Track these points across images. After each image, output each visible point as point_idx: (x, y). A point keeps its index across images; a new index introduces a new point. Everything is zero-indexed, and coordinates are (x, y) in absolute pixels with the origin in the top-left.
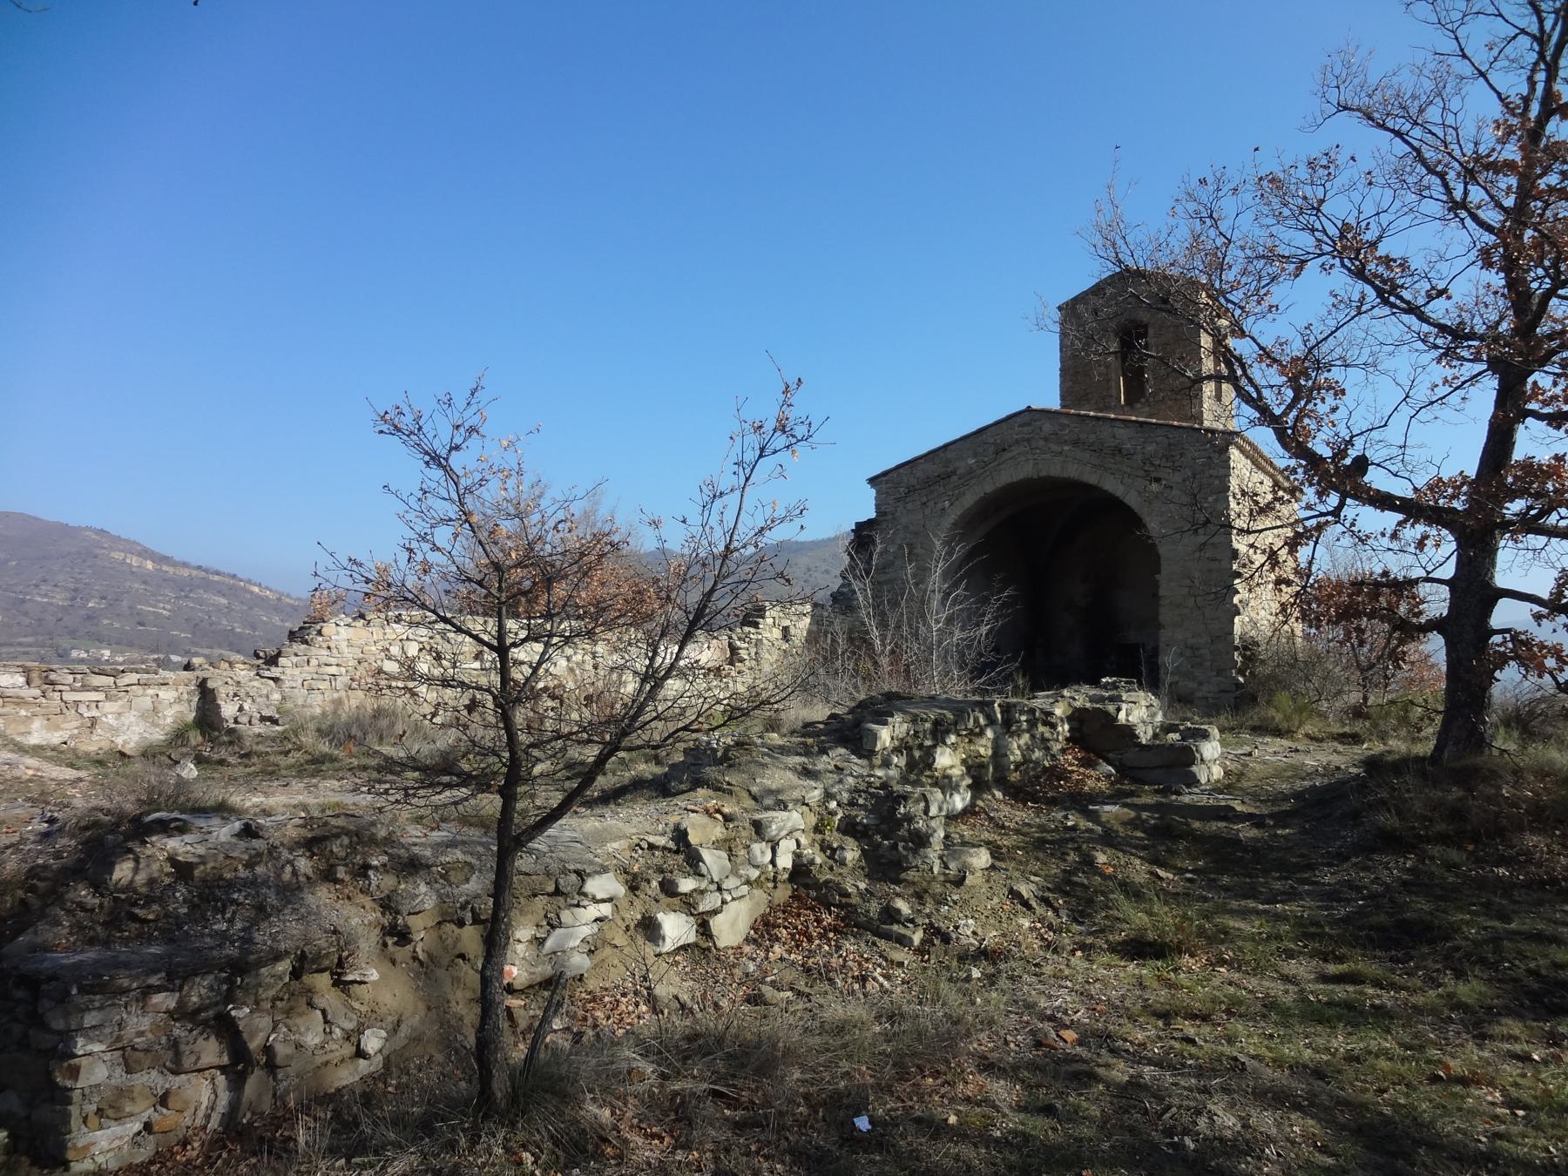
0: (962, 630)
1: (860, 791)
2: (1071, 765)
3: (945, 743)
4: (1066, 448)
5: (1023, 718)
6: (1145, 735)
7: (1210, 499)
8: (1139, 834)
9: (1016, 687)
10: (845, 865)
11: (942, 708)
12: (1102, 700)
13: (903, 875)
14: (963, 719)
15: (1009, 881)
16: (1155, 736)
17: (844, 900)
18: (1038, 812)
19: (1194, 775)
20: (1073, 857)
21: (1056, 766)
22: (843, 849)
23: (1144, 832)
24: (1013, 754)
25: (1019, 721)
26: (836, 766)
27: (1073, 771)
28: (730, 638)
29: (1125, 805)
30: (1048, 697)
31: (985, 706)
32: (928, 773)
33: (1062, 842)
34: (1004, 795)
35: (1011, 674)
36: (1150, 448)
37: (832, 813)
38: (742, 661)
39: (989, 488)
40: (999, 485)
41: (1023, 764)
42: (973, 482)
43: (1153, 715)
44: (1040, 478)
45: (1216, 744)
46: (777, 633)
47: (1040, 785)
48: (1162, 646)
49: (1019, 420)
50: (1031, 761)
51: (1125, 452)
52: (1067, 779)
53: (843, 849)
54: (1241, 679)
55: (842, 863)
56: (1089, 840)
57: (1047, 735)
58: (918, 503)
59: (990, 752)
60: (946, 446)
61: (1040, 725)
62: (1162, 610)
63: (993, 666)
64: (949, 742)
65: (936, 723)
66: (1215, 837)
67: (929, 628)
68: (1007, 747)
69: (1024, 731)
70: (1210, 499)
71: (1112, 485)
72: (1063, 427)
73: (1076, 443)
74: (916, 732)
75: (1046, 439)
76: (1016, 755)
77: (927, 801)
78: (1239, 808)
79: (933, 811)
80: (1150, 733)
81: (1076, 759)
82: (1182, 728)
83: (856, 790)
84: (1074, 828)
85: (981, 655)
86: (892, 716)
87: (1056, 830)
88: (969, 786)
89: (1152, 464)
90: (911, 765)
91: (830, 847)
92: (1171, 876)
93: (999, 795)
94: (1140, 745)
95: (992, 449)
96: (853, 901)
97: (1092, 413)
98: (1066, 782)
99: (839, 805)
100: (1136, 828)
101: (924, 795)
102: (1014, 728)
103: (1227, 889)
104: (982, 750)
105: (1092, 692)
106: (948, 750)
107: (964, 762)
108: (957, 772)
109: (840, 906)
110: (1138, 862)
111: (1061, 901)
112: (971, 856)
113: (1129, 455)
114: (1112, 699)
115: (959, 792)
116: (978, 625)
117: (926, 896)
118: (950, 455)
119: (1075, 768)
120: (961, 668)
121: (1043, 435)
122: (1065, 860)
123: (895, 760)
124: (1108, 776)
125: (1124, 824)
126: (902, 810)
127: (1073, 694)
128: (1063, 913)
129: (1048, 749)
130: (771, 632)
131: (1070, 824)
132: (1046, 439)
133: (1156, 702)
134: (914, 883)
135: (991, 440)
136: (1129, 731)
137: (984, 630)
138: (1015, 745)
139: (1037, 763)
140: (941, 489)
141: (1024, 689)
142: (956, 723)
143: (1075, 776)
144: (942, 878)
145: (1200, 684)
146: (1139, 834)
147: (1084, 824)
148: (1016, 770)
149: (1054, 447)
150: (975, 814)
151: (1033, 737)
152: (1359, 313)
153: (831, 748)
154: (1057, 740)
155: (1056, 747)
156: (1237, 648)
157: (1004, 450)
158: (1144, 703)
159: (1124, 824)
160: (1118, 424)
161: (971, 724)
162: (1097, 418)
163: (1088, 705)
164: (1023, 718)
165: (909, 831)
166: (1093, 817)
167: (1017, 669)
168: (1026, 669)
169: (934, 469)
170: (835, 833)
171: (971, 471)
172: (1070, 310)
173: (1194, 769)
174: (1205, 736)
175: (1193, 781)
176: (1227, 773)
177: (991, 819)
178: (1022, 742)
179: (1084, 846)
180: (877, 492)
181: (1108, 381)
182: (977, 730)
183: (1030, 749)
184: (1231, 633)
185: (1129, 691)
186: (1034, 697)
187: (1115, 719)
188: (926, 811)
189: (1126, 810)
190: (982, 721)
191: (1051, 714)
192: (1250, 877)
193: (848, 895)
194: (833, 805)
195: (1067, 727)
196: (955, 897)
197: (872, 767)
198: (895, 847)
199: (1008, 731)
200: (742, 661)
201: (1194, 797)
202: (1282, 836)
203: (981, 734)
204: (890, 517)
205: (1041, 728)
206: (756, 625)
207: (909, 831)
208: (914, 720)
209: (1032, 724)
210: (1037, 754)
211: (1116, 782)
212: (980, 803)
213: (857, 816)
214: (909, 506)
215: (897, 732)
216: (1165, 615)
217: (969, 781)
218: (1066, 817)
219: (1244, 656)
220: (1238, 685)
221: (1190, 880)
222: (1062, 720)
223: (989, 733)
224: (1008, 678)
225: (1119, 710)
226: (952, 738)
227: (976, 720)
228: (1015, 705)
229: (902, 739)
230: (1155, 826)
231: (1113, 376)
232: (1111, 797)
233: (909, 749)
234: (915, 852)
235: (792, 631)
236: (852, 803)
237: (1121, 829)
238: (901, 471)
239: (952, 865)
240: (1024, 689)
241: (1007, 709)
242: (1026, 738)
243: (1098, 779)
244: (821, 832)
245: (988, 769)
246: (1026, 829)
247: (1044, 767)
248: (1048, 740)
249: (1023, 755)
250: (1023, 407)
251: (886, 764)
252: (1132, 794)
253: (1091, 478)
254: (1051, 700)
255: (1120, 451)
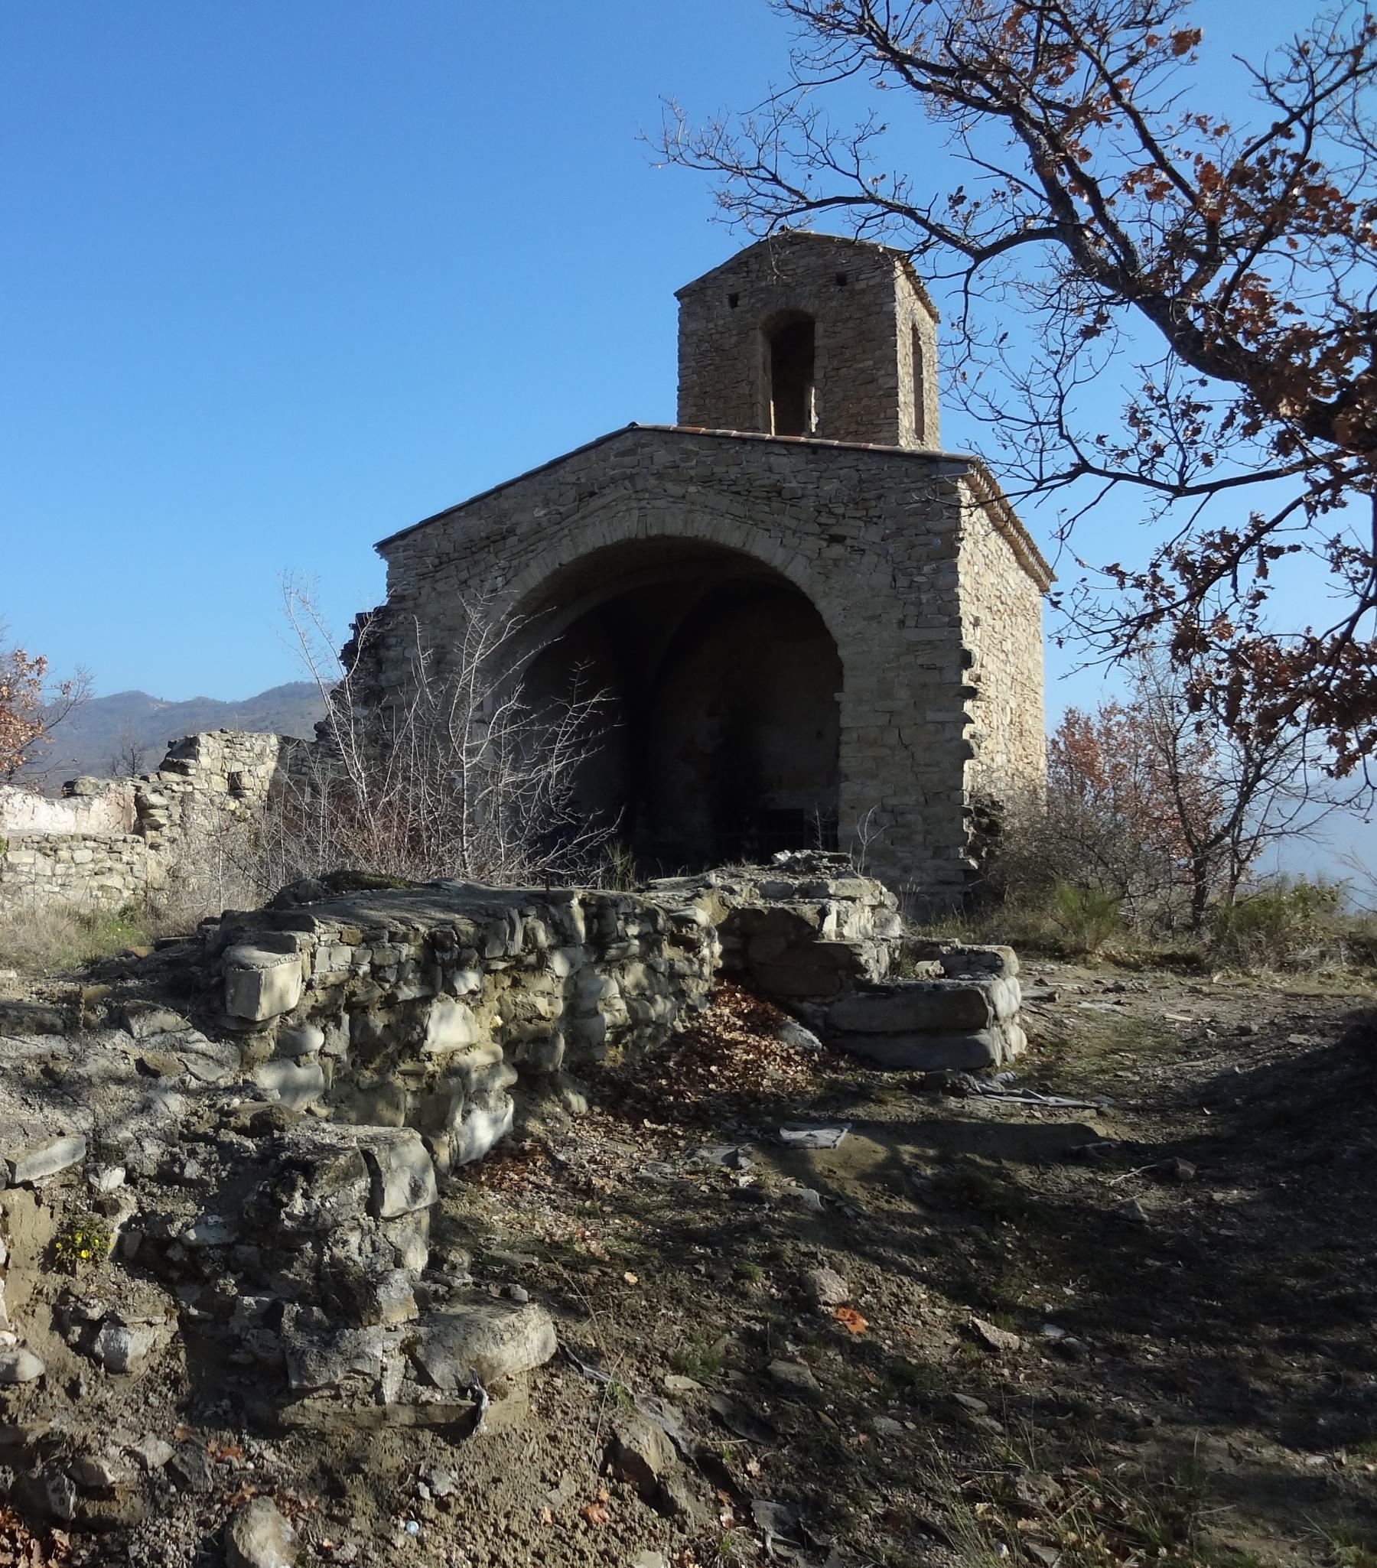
0: (515, 769)
1: (197, 1137)
2: (729, 1027)
3: (452, 992)
4: (692, 489)
5: (633, 930)
6: (876, 963)
7: (926, 569)
8: (907, 1207)
9: (612, 870)
10: (124, 1371)
11: (448, 908)
12: (786, 893)
13: (290, 1413)
14: (498, 934)
15: (605, 1413)
16: (894, 967)
17: (92, 1509)
18: (667, 1143)
19: (984, 1051)
20: (760, 1285)
21: (699, 1032)
22: (118, 1323)
23: (915, 1199)
24: (609, 1005)
25: (623, 938)
26: (141, 1064)
27: (734, 1043)
28: (138, 789)
29: (860, 1127)
30: (676, 886)
31: (549, 904)
32: (408, 1065)
33: (726, 1239)
34: (590, 1103)
35: (601, 846)
36: (829, 487)
37: (106, 1207)
38: (157, 827)
39: (566, 554)
40: (582, 550)
41: (630, 1029)
42: (543, 545)
43: (883, 924)
44: (650, 539)
45: (1013, 982)
46: (220, 785)
47: (667, 1074)
48: (843, 807)
49: (616, 445)
50: (648, 1022)
51: (786, 494)
52: (724, 1061)
53: (118, 1323)
54: (973, 863)
55: (114, 1365)
56: (796, 1231)
57: (681, 966)
58: (455, 581)
59: (560, 1007)
60: (499, 490)
61: (665, 946)
62: (844, 751)
63: (570, 831)
64: (462, 989)
65: (433, 944)
66: (1075, 1210)
67: (457, 764)
68: (598, 993)
69: (632, 958)
70: (926, 569)
71: (765, 548)
72: (688, 455)
73: (706, 481)
74: (376, 970)
75: (659, 476)
76: (615, 1011)
77: (376, 1174)
78: (1101, 1130)
79: (395, 1198)
80: (885, 960)
81: (739, 1015)
82: (945, 949)
83: (189, 1135)
84: (754, 1195)
85: (550, 813)
86: (309, 928)
87: (712, 1201)
88: (509, 1089)
89: (830, 513)
90: (363, 1047)
91: (80, 1318)
92: (1014, 1340)
93: (578, 1102)
94: (868, 985)
95: (572, 493)
96: (121, 1510)
97: (734, 433)
98: (723, 1067)
99: (130, 1179)
100: (895, 1190)
101: (368, 1156)
102: (613, 952)
103: (1168, 1383)
104: (542, 1005)
105: (765, 878)
106: (460, 1008)
107: (498, 1032)
108: (479, 1058)
109: (81, 1527)
110: (920, 1293)
111: (753, 1466)
112: (498, 1339)
113: (795, 500)
114: (806, 892)
115: (485, 1106)
116: (543, 759)
117: (354, 1485)
118: (505, 504)
119: (736, 1035)
120: (512, 837)
121: (654, 468)
122: (745, 1295)
123: (316, 1038)
124: (807, 1052)
125: (864, 1177)
126: (298, 1205)
127: (728, 882)
128: (764, 1512)
129: (681, 994)
130: (209, 782)
131: (744, 1181)
132: (659, 476)
133: (890, 899)
134: (322, 1436)
135: (572, 479)
136: (845, 957)
137: (555, 768)
138: (614, 989)
139: (659, 1025)
140: (492, 558)
141: (625, 874)
142: (481, 945)
143: (739, 1055)
144: (406, 1416)
145: (906, 870)
146: (907, 1207)
147: (779, 1183)
148: (616, 1042)
149: (675, 490)
150: (522, 1157)
151: (651, 969)
152: (1353, 73)
153: (137, 1012)
154: (700, 976)
155: (697, 989)
156: (967, 813)
157: (592, 494)
158: (868, 900)
159: (864, 1177)
160: (777, 449)
161: (517, 946)
162: (743, 441)
163: (759, 903)
164: (633, 930)
165: (317, 1267)
166: (791, 1159)
167: (612, 837)
168: (626, 838)
169: (479, 526)
170: (107, 1267)
171: (538, 529)
172: (692, 296)
173: (983, 1037)
174: (995, 967)
175: (980, 1062)
176: (1035, 1041)
177: (559, 1169)
178: (629, 981)
179: (788, 1247)
180: (392, 566)
181: (753, 405)
182: (532, 959)
183: (640, 997)
184: (958, 787)
185: (839, 876)
186: (649, 888)
187: (818, 932)
188: (373, 1203)
189: (865, 1141)
190: (543, 938)
191: (688, 921)
192: (1212, 1342)
193: (106, 1493)
194: (113, 1179)
195: (718, 948)
196: (444, 1485)
197: (247, 1062)
198: (271, 1316)
199: (600, 959)
200: (157, 827)
201: (994, 1101)
202: (1230, 1208)
203: (541, 965)
204: (410, 604)
205: (668, 952)
206: (183, 770)
207: (317, 1267)
208: (370, 939)
209: (652, 942)
210: (661, 1006)
211: (825, 1064)
212: (534, 1126)
213: (170, 1218)
214: (441, 586)
215: (322, 968)
216: (850, 758)
217: (508, 1077)
218: (732, 1161)
219: (977, 826)
220: (969, 872)
221: (1059, 1350)
222: (709, 934)
223: (559, 965)
224: (595, 855)
225: (823, 913)
226: (471, 980)
227: (529, 937)
228: (615, 903)
229: (338, 987)
230: (936, 1185)
231: (760, 398)
232: (819, 1103)
233: (358, 1009)
234: (328, 1341)
235: (246, 781)
236: (168, 1175)
237: (862, 1195)
238: (429, 530)
239: (440, 1371)
240: (625, 874)
241: (597, 911)
242: (636, 972)
243: (788, 1060)
244: (62, 1268)
245: (555, 1046)
246: (641, 1198)
247: (675, 1034)
248: (683, 976)
249: (631, 1009)
250: (624, 424)
251: (290, 1050)
252: (862, 1094)
253: (731, 537)
254: (686, 894)
255: (779, 493)
